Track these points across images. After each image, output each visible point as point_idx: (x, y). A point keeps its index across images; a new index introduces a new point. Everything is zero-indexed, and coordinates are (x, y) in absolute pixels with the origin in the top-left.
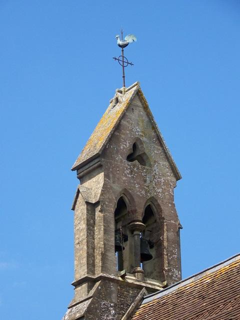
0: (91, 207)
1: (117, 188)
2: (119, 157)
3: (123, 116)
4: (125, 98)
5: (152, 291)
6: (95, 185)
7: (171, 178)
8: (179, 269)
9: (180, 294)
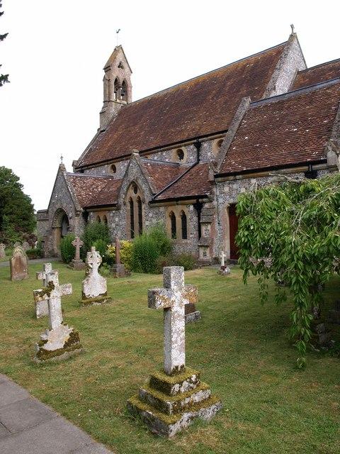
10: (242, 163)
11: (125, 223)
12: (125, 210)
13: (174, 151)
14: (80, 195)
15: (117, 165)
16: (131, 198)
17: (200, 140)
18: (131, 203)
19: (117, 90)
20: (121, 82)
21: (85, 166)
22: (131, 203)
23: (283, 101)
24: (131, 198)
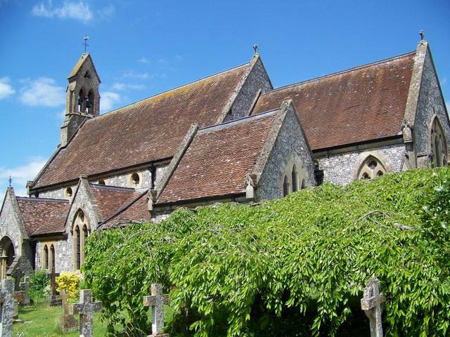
0: (72, 92)
1: (80, 86)
2: (81, 76)
3: (84, 63)
4: (85, 57)
5: (90, 118)
6: (74, 84)
7: (98, 83)
8: (99, 111)
9: (95, 121)
10: (179, 194)
11: (72, 252)
12: (72, 239)
13: (66, 189)
14: (29, 222)
15: (140, 174)
16: (77, 226)
17: (154, 164)
18: (78, 231)
19: (82, 101)
20: (87, 93)
21: (39, 188)
22: (78, 231)
23: (226, 130)
24: (77, 226)
